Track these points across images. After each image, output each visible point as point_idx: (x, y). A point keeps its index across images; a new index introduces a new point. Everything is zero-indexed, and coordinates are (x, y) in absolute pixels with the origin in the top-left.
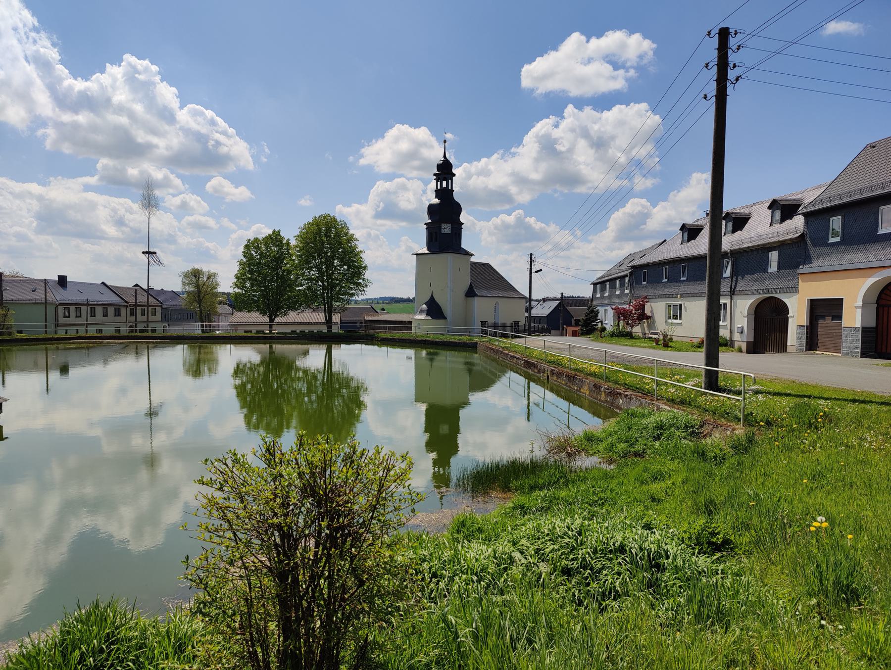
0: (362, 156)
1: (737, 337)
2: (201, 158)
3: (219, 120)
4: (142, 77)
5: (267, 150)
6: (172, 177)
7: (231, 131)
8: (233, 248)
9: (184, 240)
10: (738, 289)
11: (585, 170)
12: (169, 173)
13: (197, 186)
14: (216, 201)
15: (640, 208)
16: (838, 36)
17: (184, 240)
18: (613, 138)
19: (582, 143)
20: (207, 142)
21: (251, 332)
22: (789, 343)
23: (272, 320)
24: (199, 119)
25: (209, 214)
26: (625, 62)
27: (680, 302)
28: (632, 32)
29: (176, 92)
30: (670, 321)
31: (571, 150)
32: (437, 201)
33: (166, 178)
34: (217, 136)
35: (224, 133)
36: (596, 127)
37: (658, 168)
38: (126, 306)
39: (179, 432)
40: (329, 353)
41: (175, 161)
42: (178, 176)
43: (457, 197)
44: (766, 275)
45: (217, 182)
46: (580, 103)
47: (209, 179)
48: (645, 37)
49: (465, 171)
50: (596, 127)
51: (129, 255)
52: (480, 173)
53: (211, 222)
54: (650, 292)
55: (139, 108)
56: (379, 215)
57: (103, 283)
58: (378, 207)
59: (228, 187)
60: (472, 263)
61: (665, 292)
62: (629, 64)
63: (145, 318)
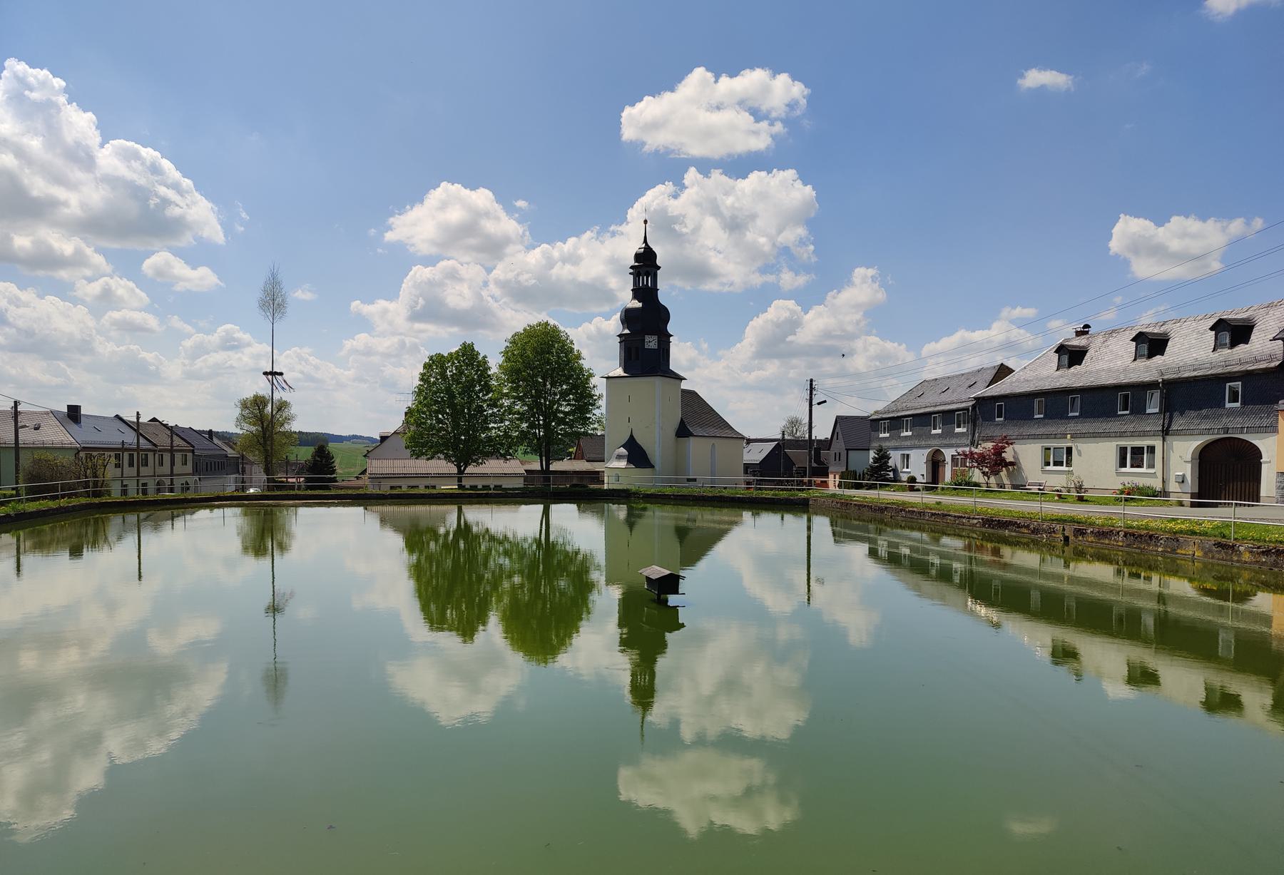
0: (390, 228)
1: (1173, 487)
2: (135, 224)
3: (166, 164)
4: (35, 96)
5: (244, 215)
6: (89, 251)
7: (187, 183)
8: (187, 362)
9: (106, 348)
10: (1174, 427)
11: (715, 260)
12: (83, 245)
13: (128, 266)
14: (161, 293)
15: (787, 314)
16: (1041, 92)
17: (106, 348)
18: (753, 217)
19: (710, 222)
20: (147, 199)
21: (434, 487)
22: (1263, 493)
23: (460, 472)
24: (136, 165)
25: (147, 309)
26: (769, 112)
27: (1069, 445)
28: (776, 72)
29: (94, 117)
30: (1048, 468)
31: (696, 230)
32: (638, 305)
33: (78, 252)
34: (162, 190)
35: (176, 187)
36: (730, 201)
37: (814, 259)
38: (154, 451)
39: (100, 647)
40: (546, 513)
41: (92, 226)
42: (98, 251)
43: (663, 299)
44: (1220, 411)
45: (159, 259)
46: (705, 166)
47: (149, 254)
48: (794, 78)
49: (543, 253)
50: (730, 201)
51: (14, 372)
52: (566, 260)
53: (152, 322)
54: (1011, 431)
55: (35, 144)
56: (415, 316)
57: (117, 416)
58: (417, 303)
59: (180, 268)
60: (684, 391)
61: (1041, 430)
62: (774, 115)
63: (133, 471)
